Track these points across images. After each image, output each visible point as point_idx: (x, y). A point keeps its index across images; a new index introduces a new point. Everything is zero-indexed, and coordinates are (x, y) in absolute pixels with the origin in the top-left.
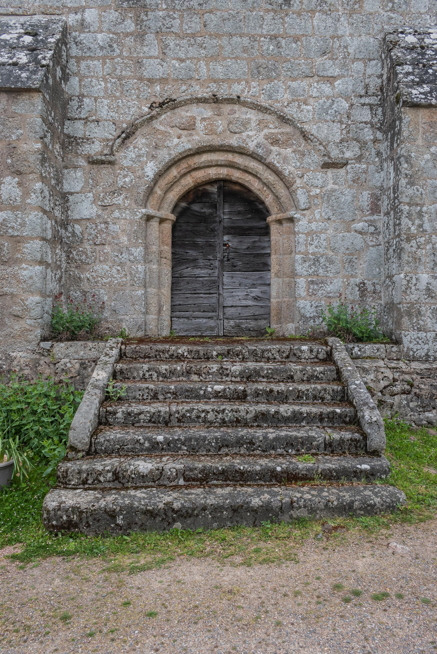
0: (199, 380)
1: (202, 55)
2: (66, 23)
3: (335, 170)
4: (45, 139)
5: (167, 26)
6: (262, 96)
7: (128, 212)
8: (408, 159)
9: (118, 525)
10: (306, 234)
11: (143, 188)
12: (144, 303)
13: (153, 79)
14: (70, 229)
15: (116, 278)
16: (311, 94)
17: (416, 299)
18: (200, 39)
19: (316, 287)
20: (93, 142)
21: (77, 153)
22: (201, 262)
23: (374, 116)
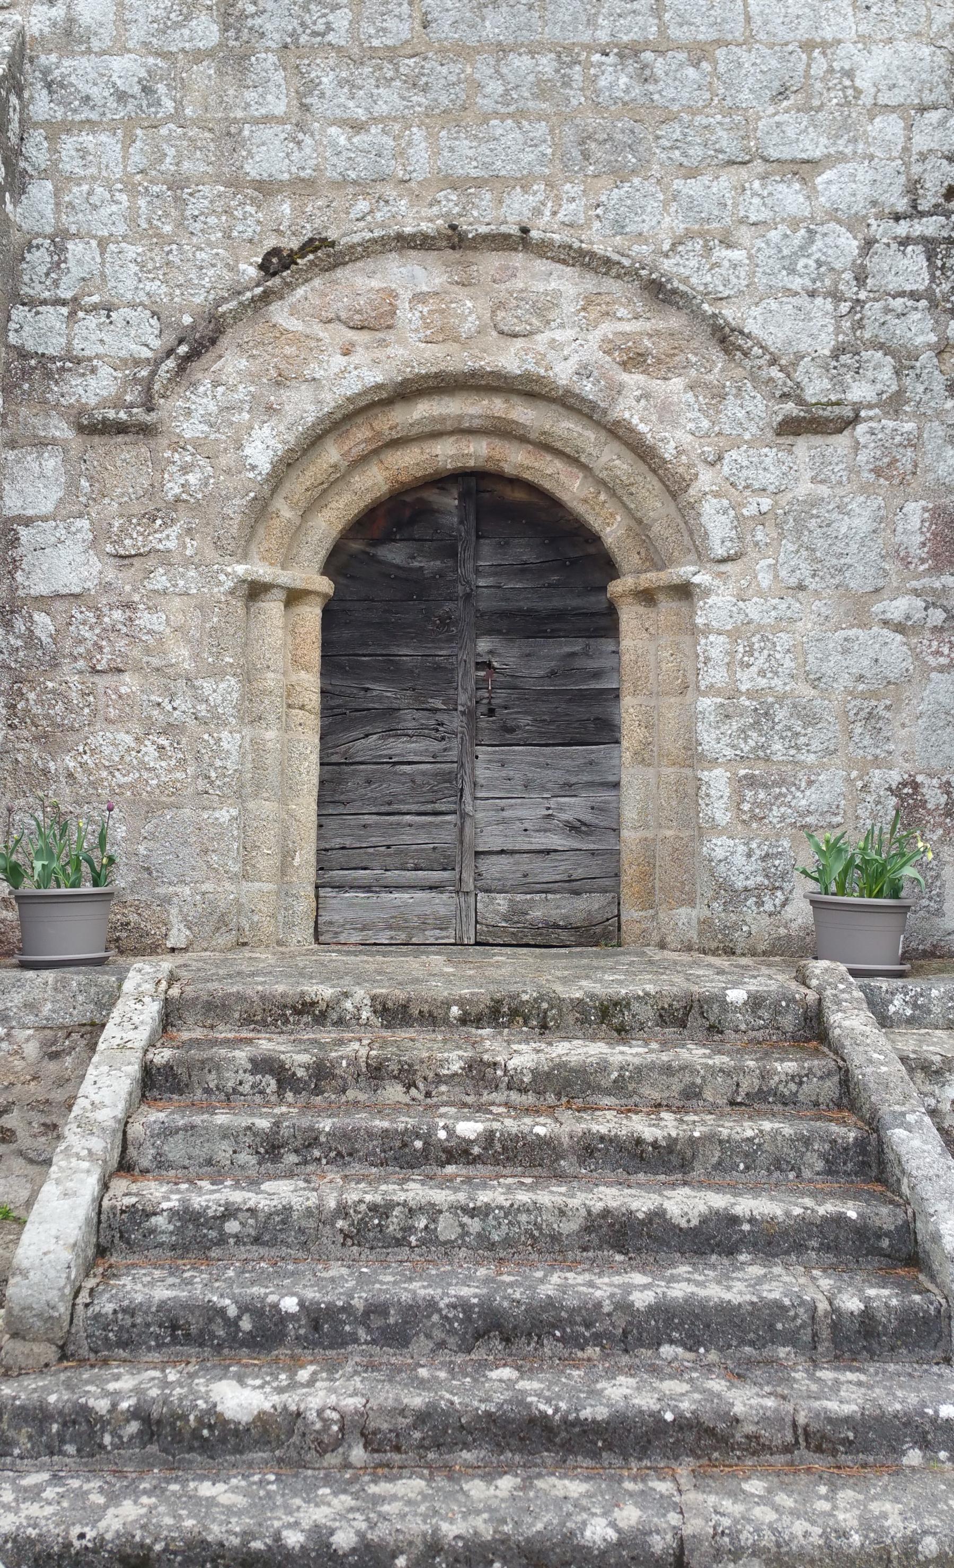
0: (406, 1099)
2: (21, 34)
3: (818, 440)
5: (316, 28)
6: (597, 225)
7: (192, 573)
10: (728, 633)
13: (271, 183)
14: (20, 625)
15: (155, 769)
16: (742, 214)
18: (411, 62)
19: (762, 795)
20: (93, 371)
21: (46, 402)
22: (410, 719)
23: (938, 273)
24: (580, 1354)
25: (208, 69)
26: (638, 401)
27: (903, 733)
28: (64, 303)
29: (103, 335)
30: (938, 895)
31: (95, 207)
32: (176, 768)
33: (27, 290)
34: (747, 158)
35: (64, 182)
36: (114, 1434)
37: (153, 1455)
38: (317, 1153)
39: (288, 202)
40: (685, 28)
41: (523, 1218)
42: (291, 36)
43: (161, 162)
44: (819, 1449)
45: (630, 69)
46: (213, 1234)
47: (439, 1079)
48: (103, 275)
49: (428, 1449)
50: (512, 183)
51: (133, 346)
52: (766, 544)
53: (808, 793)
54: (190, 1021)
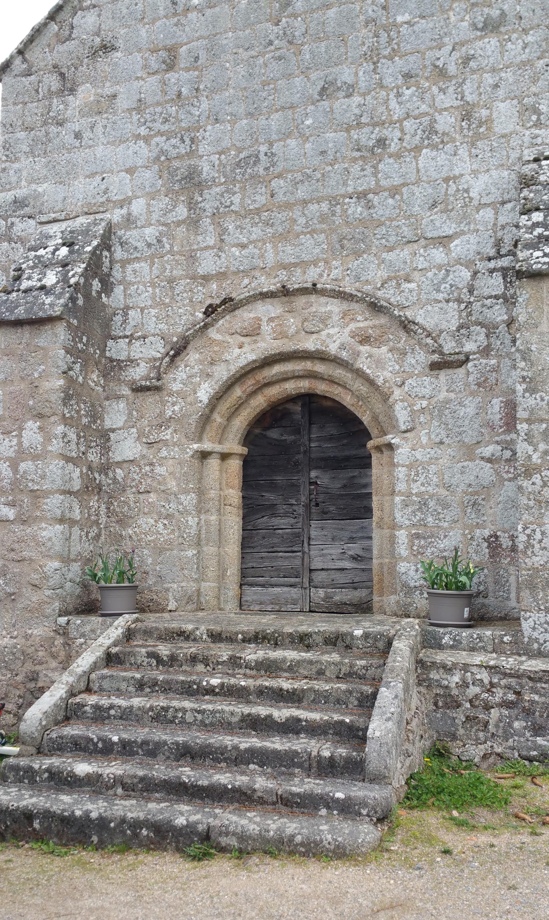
0: (205, 671)
1: (269, 235)
3: (450, 371)
4: (71, 373)
5: (226, 204)
6: (347, 278)
7: (176, 449)
8: (526, 355)
9: (34, 830)
10: (407, 466)
11: (194, 417)
12: (195, 566)
13: (208, 276)
14: (111, 475)
15: (162, 534)
16: (415, 266)
17: (542, 563)
18: (266, 214)
19: (422, 542)
20: (138, 365)
21: (120, 380)
22: (282, 509)
23: (508, 285)
24: (218, 765)
25: (183, 228)
26: (367, 359)
27: (491, 511)
28: (126, 337)
29: (142, 349)
30: (508, 590)
31: (139, 295)
32: (170, 533)
33: (114, 333)
34: (417, 239)
35: (127, 285)
36: (40, 777)
37: (52, 786)
38: (157, 688)
39: (215, 283)
40: (388, 180)
41: (218, 715)
42: (216, 209)
43: (165, 272)
44: (286, 805)
45: (362, 204)
46: (106, 714)
47: (218, 663)
48: (142, 323)
49: (144, 791)
50: (310, 263)
51: (153, 353)
52: (425, 423)
53: (444, 541)
54: (138, 637)
